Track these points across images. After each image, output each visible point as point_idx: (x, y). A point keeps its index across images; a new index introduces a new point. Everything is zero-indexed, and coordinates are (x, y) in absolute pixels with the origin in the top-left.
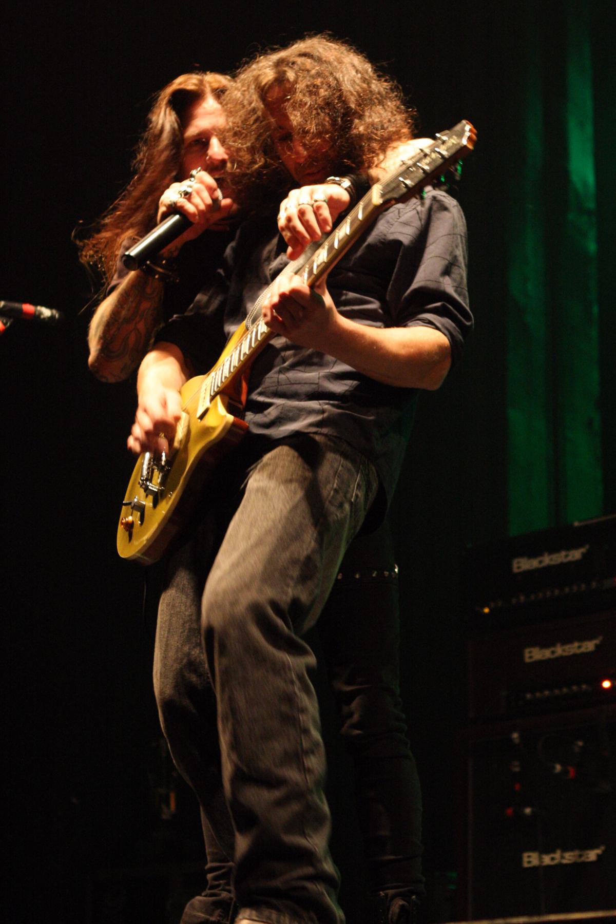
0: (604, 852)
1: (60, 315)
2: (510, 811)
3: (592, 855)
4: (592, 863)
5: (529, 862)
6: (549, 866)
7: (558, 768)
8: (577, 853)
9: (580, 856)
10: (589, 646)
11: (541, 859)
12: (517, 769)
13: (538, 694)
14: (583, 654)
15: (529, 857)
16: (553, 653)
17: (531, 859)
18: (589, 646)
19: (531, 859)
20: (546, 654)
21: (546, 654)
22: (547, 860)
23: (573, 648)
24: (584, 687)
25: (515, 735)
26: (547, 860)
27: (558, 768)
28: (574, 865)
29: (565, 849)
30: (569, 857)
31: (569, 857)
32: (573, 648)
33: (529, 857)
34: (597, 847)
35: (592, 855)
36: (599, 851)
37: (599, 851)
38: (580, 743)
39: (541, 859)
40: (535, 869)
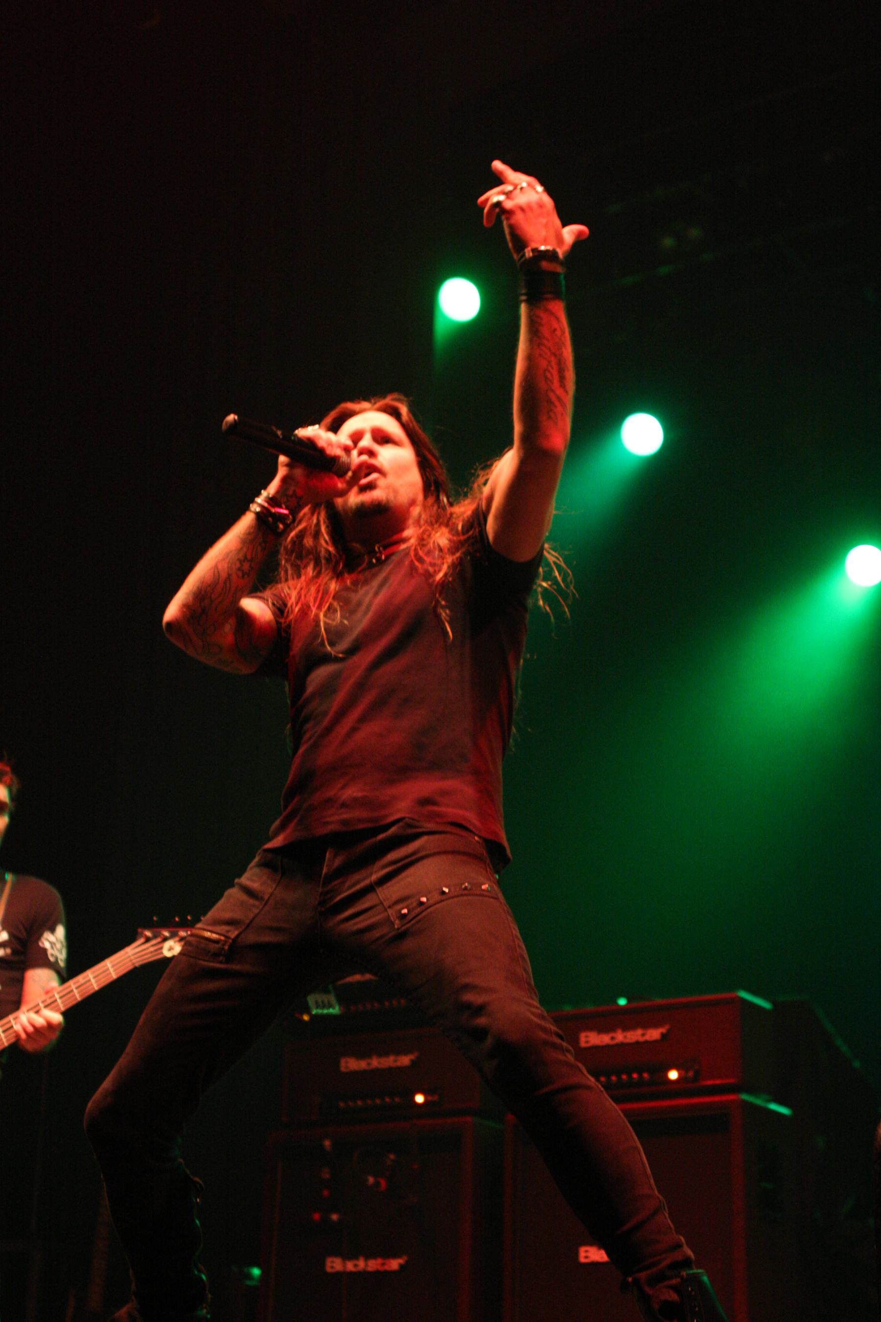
0: (407, 1262)
1: (235, 413)
2: (316, 1216)
3: (395, 1264)
4: (394, 1272)
5: (586, 1257)
6: (351, 1273)
7: (371, 1180)
8: (380, 1261)
9: (383, 1264)
10: (405, 1060)
11: (344, 1265)
12: (327, 1176)
13: (369, 1102)
14: (646, 1042)
15: (587, 1251)
16: (613, 1038)
17: (335, 1264)
18: (405, 1060)
19: (335, 1264)
20: (605, 1039)
21: (605, 1039)
22: (350, 1266)
23: (389, 1061)
24: (397, 1100)
25: (327, 1143)
26: (350, 1266)
27: (371, 1180)
28: (377, 1273)
29: (367, 1257)
30: (373, 1265)
31: (373, 1265)
32: (389, 1061)
33: (587, 1251)
34: (399, 1257)
35: (395, 1264)
36: (401, 1261)
37: (401, 1261)
38: (392, 1157)
39: (344, 1265)
40: (338, 1275)
